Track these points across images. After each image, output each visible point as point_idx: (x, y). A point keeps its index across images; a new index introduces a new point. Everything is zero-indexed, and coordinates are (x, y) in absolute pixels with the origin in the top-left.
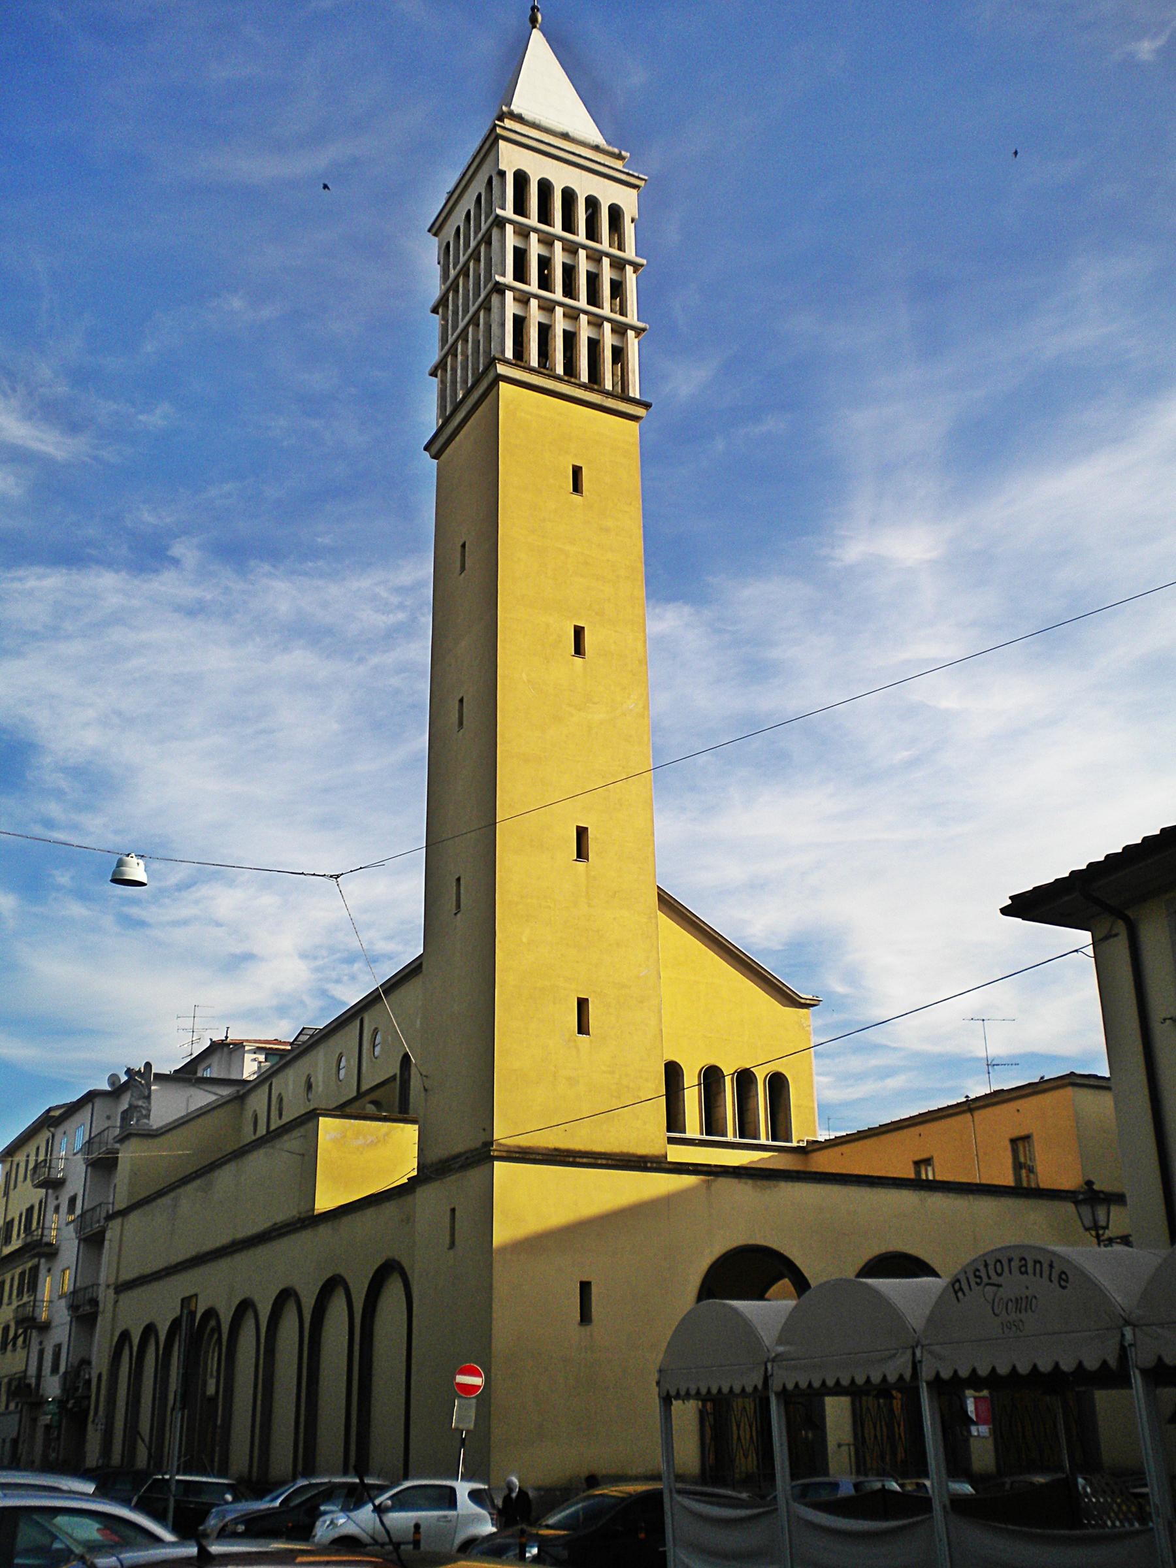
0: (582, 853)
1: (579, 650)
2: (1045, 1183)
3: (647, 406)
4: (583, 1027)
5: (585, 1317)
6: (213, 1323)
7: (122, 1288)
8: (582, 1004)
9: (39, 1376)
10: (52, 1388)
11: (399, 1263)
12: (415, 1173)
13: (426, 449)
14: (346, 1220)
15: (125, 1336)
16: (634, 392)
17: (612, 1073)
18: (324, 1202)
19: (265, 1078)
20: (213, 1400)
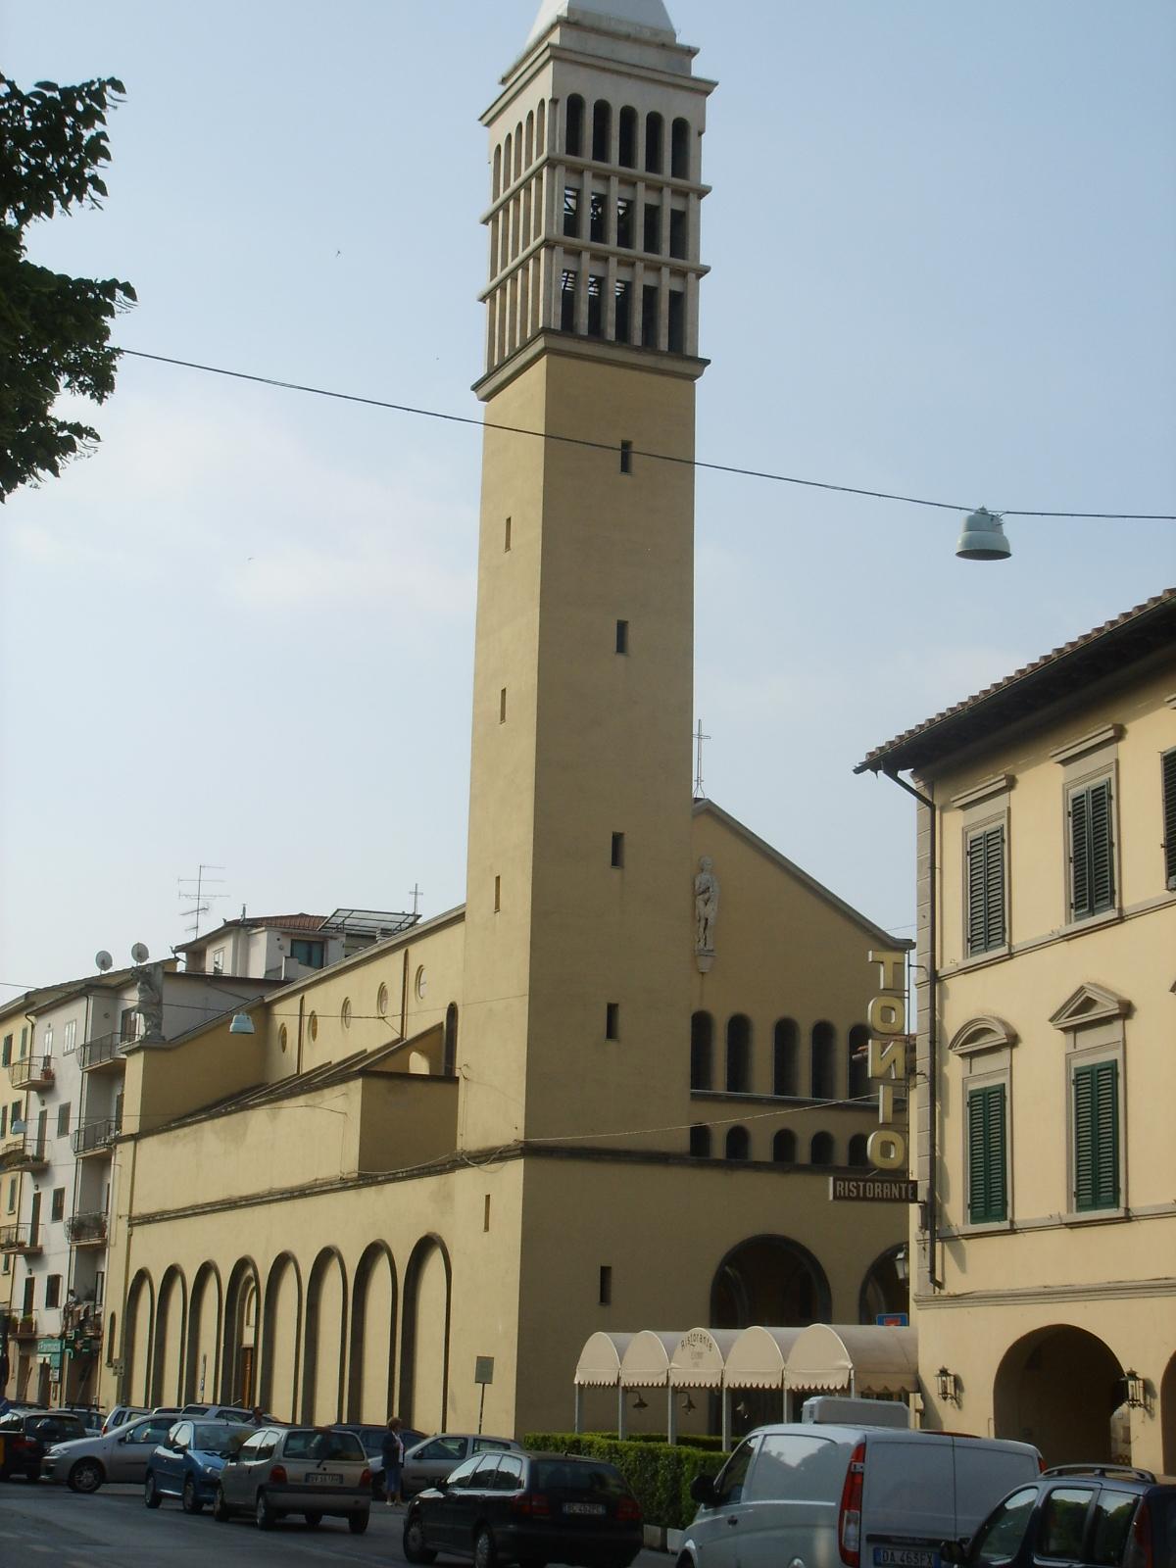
0: (616, 860)
2: (945, 1430)
4: (611, 1032)
6: (250, 1272)
7: (135, 1221)
8: (612, 1009)
9: (41, 1140)
10: (49, 1322)
15: (143, 1275)
20: (253, 1350)
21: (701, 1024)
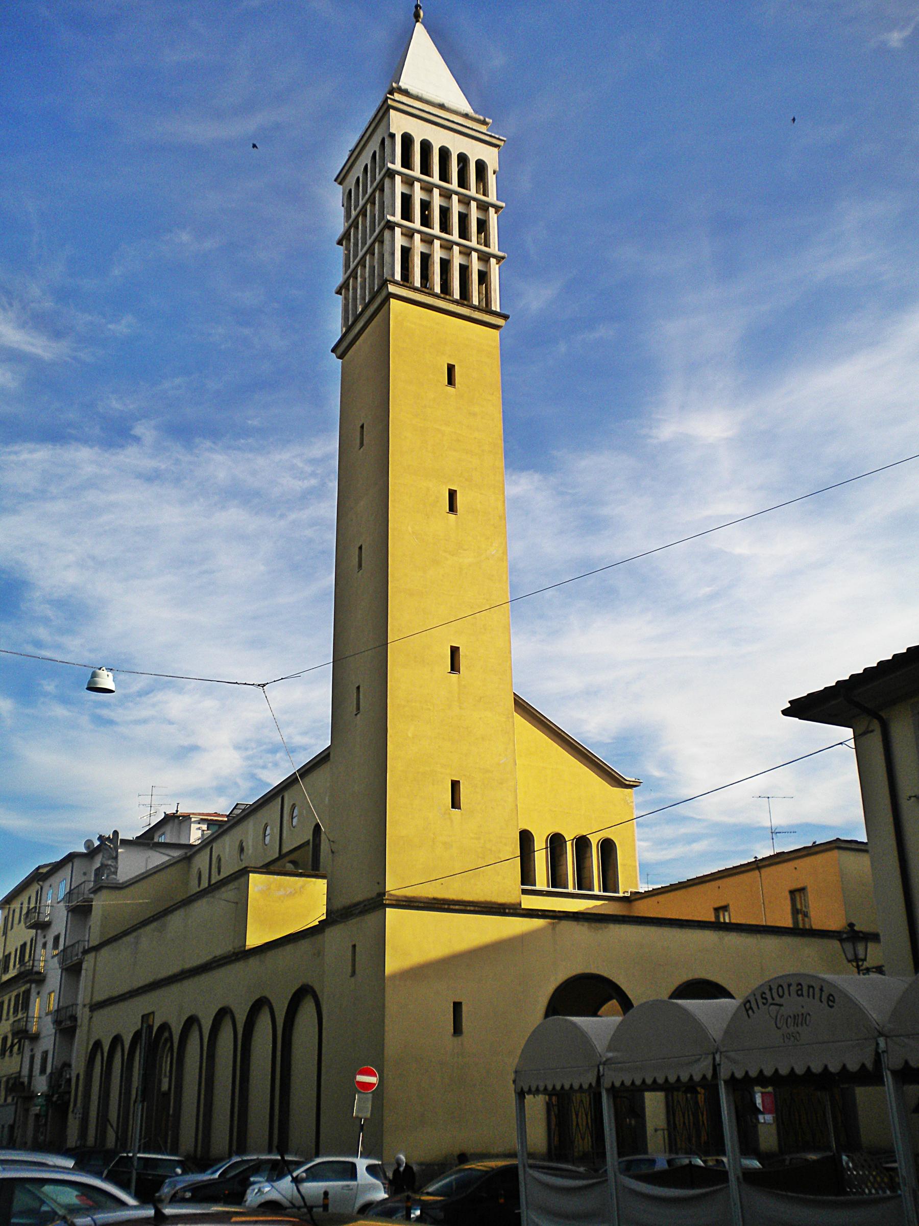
0: (455, 667)
1: (452, 508)
3: (505, 317)
4: (455, 803)
5: (457, 1030)
6: (166, 1034)
7: (95, 1007)
8: (455, 785)
10: (41, 1085)
11: (312, 988)
12: (324, 917)
13: (333, 351)
14: (271, 954)
15: (98, 1044)
16: (496, 306)
17: (478, 839)
18: (254, 940)
19: (207, 843)
20: (167, 1094)
21: (526, 838)
